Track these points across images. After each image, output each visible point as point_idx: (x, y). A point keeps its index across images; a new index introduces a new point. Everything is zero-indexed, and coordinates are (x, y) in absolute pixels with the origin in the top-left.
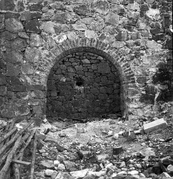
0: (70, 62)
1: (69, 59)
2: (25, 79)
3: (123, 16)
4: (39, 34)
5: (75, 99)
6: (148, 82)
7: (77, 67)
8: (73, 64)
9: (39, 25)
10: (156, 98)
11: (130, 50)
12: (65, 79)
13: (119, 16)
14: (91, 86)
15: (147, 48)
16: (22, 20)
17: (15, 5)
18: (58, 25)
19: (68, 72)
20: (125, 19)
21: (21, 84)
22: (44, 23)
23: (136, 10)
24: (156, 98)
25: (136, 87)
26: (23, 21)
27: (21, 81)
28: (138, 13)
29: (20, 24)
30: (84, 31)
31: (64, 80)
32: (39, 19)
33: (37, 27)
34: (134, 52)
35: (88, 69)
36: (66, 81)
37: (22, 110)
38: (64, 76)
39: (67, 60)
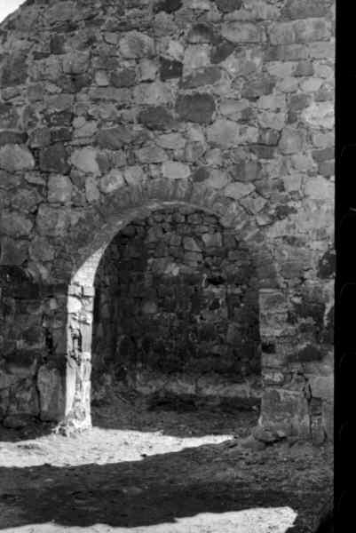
0: (190, 224)
1: (189, 218)
2: (37, 270)
3: (249, 125)
4: (65, 175)
5: (203, 321)
6: (306, 275)
7: (206, 238)
8: (196, 230)
9: (67, 156)
10: (327, 312)
11: (265, 201)
12: (178, 268)
13: (239, 127)
14: (245, 287)
15: (305, 196)
16: (33, 146)
17: (18, 117)
18: (103, 153)
19: (185, 251)
20: (252, 134)
21: (29, 280)
22: (77, 151)
23: (278, 110)
24: (327, 312)
25: (278, 287)
26: (35, 149)
27: (28, 275)
28: (283, 116)
29: (29, 155)
30: (161, 163)
31: (176, 272)
32: (66, 144)
33: (62, 160)
34: (274, 206)
35: (237, 242)
36: (180, 273)
37: (29, 337)
38: (174, 261)
39: (183, 220)
